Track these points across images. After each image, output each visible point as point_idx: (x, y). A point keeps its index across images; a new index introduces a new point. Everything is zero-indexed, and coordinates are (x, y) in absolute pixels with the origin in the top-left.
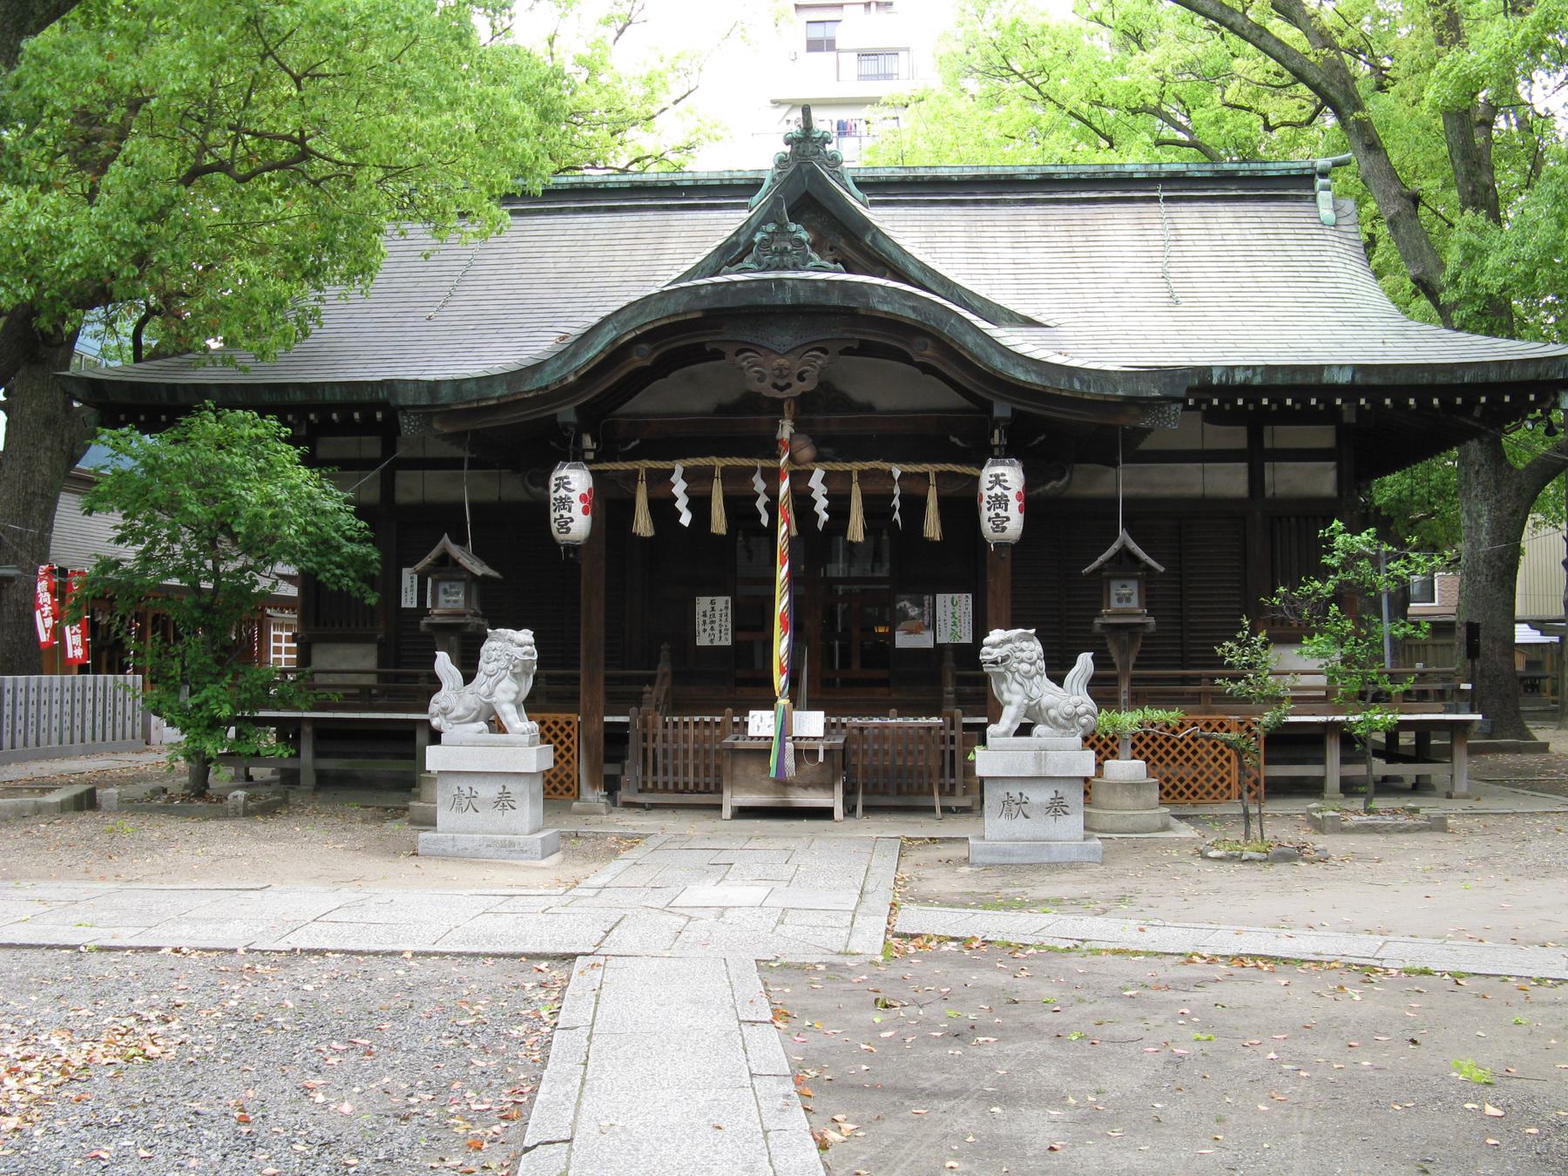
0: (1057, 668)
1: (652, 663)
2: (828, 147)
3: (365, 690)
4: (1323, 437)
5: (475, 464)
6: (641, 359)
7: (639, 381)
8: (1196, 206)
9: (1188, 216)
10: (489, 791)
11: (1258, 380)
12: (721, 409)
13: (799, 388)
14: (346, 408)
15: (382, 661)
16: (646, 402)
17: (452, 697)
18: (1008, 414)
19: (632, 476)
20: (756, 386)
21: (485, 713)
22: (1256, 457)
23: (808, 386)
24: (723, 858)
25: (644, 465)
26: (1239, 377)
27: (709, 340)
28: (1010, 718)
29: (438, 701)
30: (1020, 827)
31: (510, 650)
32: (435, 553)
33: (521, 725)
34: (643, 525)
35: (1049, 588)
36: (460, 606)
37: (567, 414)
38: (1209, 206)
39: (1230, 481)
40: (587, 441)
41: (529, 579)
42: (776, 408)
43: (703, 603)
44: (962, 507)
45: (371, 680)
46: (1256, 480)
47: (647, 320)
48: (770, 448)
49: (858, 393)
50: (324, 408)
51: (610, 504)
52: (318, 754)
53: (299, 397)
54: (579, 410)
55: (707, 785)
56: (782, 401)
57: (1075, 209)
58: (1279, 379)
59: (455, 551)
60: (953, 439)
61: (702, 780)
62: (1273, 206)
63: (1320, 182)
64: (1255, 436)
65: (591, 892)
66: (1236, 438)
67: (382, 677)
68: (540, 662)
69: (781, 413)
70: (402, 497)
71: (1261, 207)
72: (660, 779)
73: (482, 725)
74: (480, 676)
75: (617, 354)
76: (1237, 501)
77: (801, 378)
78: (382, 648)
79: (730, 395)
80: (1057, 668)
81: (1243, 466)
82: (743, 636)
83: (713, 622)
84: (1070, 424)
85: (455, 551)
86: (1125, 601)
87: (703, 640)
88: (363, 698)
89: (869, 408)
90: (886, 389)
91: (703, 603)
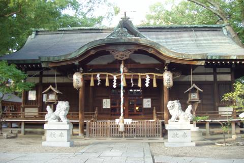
0: (184, 108)
1: (94, 111)
2: (129, 20)
3: (35, 116)
4: (228, 70)
5: (57, 76)
6: (92, 53)
7: (92, 57)
8: (200, 32)
9: (199, 34)
10: (58, 133)
11: (217, 58)
12: (108, 64)
13: (125, 58)
14: (32, 64)
15: (39, 111)
16: (93, 63)
17: (50, 115)
18: (169, 62)
19: (90, 76)
20: (116, 58)
21: (57, 120)
22: (215, 74)
23: (127, 57)
24: (110, 146)
25: (92, 74)
26: (214, 58)
27: (107, 49)
28: (173, 118)
29: (47, 116)
30: (176, 139)
31: (63, 106)
32: (49, 88)
33: (65, 121)
34: (92, 84)
35: (179, 92)
36: (54, 99)
37: (76, 63)
38: (202, 32)
39: (210, 78)
40: (81, 69)
41: (67, 93)
42: (120, 62)
43: (104, 100)
44: (160, 81)
45: (37, 114)
46: (215, 78)
47: (94, 45)
48: (118, 71)
49: (137, 61)
50: (27, 64)
51: (86, 82)
52: (25, 128)
53: (22, 62)
54: (79, 62)
55: (149, 136)
56: (121, 61)
57: (176, 33)
58: (222, 58)
59: (53, 89)
60: (157, 69)
61: (151, 135)
62: (215, 32)
63: (223, 28)
64: (215, 70)
65: (80, 154)
66: (211, 70)
67: (39, 114)
68: (70, 108)
69: (121, 63)
70: (44, 82)
71: (212, 32)
72: (114, 134)
73: (57, 120)
74: (57, 110)
75: (87, 52)
76: (212, 81)
77: (126, 56)
78: (39, 108)
79: (111, 61)
80: (184, 108)
81: (212, 75)
82: (113, 106)
83: (107, 104)
84: (180, 68)
85: (53, 89)
86: (194, 97)
87: (104, 107)
88: (35, 117)
89: (139, 63)
90: (143, 60)
91: (104, 100)
